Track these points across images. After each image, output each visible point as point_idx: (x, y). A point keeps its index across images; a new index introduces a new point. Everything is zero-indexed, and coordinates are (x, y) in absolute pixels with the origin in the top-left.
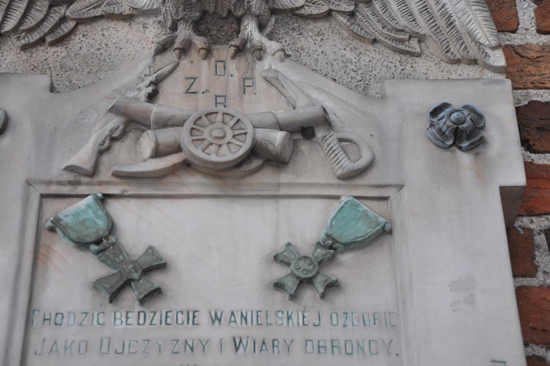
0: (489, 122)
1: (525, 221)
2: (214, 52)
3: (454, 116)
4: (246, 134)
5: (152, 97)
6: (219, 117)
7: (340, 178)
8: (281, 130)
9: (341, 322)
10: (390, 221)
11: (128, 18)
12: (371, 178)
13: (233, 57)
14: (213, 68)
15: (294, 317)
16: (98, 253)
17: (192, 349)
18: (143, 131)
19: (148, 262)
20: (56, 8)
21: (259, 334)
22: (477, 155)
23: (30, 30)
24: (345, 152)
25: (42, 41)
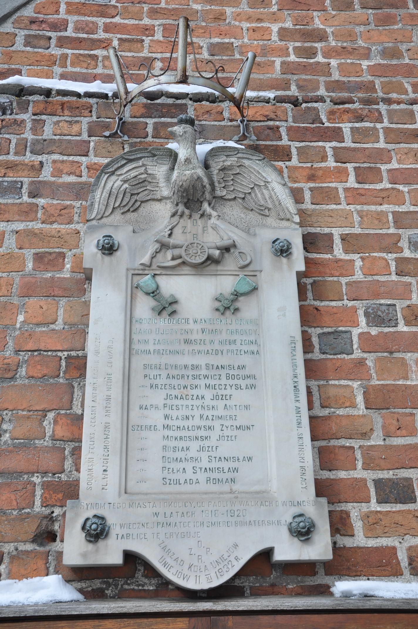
1: (304, 280)
2: (193, 216)
3: (281, 244)
5: (170, 235)
6: (195, 245)
7: (239, 268)
8: (218, 250)
9: (239, 323)
10: (257, 285)
11: (160, 200)
12: (251, 268)
13: (200, 218)
14: (192, 222)
17: (187, 333)
18: (168, 249)
19: (170, 300)
20: (133, 196)
21: (211, 327)
22: (288, 258)
23: (125, 206)
24: (241, 258)
25: (129, 210)
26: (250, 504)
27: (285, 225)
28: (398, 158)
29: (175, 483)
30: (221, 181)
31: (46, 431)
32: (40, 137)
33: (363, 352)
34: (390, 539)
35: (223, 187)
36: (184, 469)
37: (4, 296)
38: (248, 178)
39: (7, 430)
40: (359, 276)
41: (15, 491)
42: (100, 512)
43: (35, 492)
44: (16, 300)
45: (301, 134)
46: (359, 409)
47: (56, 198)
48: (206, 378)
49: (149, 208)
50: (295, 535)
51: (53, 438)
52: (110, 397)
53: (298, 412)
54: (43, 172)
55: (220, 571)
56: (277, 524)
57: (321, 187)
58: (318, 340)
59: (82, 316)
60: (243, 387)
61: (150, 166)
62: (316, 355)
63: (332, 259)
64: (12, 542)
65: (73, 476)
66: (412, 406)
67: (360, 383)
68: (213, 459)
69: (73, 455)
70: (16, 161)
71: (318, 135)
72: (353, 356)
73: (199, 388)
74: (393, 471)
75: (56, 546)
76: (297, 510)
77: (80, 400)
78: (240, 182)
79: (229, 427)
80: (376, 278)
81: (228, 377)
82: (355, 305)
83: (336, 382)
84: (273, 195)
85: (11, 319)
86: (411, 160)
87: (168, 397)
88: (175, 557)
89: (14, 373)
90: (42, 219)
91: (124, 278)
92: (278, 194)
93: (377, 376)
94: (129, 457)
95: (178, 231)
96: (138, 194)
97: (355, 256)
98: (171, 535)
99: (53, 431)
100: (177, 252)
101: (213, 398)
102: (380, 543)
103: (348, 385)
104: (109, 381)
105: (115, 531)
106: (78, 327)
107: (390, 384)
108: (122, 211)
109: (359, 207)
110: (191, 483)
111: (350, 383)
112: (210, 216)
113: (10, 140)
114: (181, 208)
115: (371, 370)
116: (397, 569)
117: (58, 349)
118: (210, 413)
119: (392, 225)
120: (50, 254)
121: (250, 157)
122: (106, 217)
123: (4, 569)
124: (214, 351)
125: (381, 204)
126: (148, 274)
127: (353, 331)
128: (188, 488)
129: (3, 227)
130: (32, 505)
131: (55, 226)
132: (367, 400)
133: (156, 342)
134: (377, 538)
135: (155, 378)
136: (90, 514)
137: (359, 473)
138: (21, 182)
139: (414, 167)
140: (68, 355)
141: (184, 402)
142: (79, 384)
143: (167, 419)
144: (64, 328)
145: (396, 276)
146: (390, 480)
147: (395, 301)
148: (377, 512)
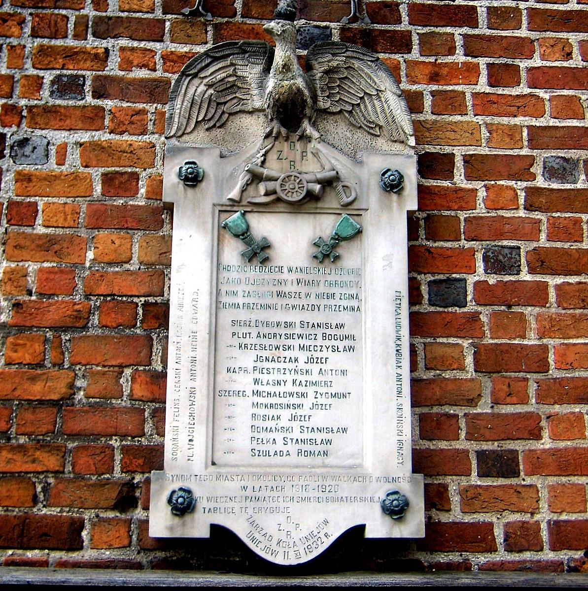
0: (405, 178)
4: (304, 187)
5: (263, 162)
6: (293, 177)
7: (342, 206)
11: (250, 113)
12: (355, 206)
15: (321, 270)
16: (243, 239)
23: (209, 120)
24: (345, 192)
25: (214, 126)
26: (342, 479)
27: (398, 149)
28: (542, 52)
29: (264, 454)
30: (325, 87)
31: (124, 390)
32: (104, 14)
33: (478, 304)
34: (487, 514)
35: (328, 97)
36: (274, 439)
37: (70, 228)
38: (358, 84)
39: (81, 387)
40: (480, 210)
41: (93, 455)
42: (186, 485)
43: (114, 457)
44: (83, 233)
45: (424, 16)
46: (467, 372)
47: (126, 100)
48: (301, 338)
49: (238, 123)
50: (388, 513)
51: (131, 397)
52: (195, 359)
53: (399, 380)
54: (109, 64)
55: (309, 547)
56: (369, 501)
57: (446, 91)
58: (428, 289)
59: (161, 254)
60: (341, 349)
61: (240, 65)
62: (425, 307)
63: (451, 188)
64: (92, 509)
65: (154, 440)
66: (527, 370)
67: (471, 341)
68: (306, 430)
69: (153, 417)
70: (77, 48)
71: (445, 17)
72: (465, 310)
73: (292, 349)
74: (499, 442)
75: (139, 513)
76: (391, 487)
77: (160, 354)
78: (347, 89)
79: (324, 394)
80: (501, 213)
81: (324, 336)
82: (473, 246)
83: (444, 340)
84: (386, 108)
85: (79, 256)
86: (557, 55)
87: (259, 359)
88: (263, 532)
89: (86, 321)
90: (110, 127)
91: (210, 216)
92: (392, 108)
93: (491, 333)
94: (215, 425)
95: (272, 157)
96: (225, 103)
97: (478, 185)
98: (260, 509)
99: (131, 390)
100: (271, 185)
101: (307, 362)
102: (476, 518)
103: (457, 344)
104: (194, 340)
105: (202, 504)
106: (156, 267)
107: (504, 343)
108: (207, 126)
109: (488, 119)
110: (281, 455)
111: (460, 341)
112: (309, 139)
113: (68, 18)
114: (276, 125)
115: (484, 327)
116: (491, 546)
117: (134, 293)
118: (303, 378)
119: (526, 143)
120: (122, 174)
121: (362, 57)
122: (187, 134)
123: (86, 535)
124: (310, 306)
125: (515, 116)
126: (238, 211)
127: (468, 279)
128: (278, 459)
129: (64, 137)
130: (111, 470)
131: (126, 137)
132: (477, 362)
133: (246, 295)
134: (474, 513)
135: (244, 336)
136: (176, 486)
137: (462, 444)
138: (84, 77)
139: (560, 66)
140: (145, 301)
141: (276, 365)
142: (159, 336)
143: (256, 383)
144: (139, 269)
145: (523, 211)
146: (494, 452)
147: (520, 242)
148: (477, 486)
